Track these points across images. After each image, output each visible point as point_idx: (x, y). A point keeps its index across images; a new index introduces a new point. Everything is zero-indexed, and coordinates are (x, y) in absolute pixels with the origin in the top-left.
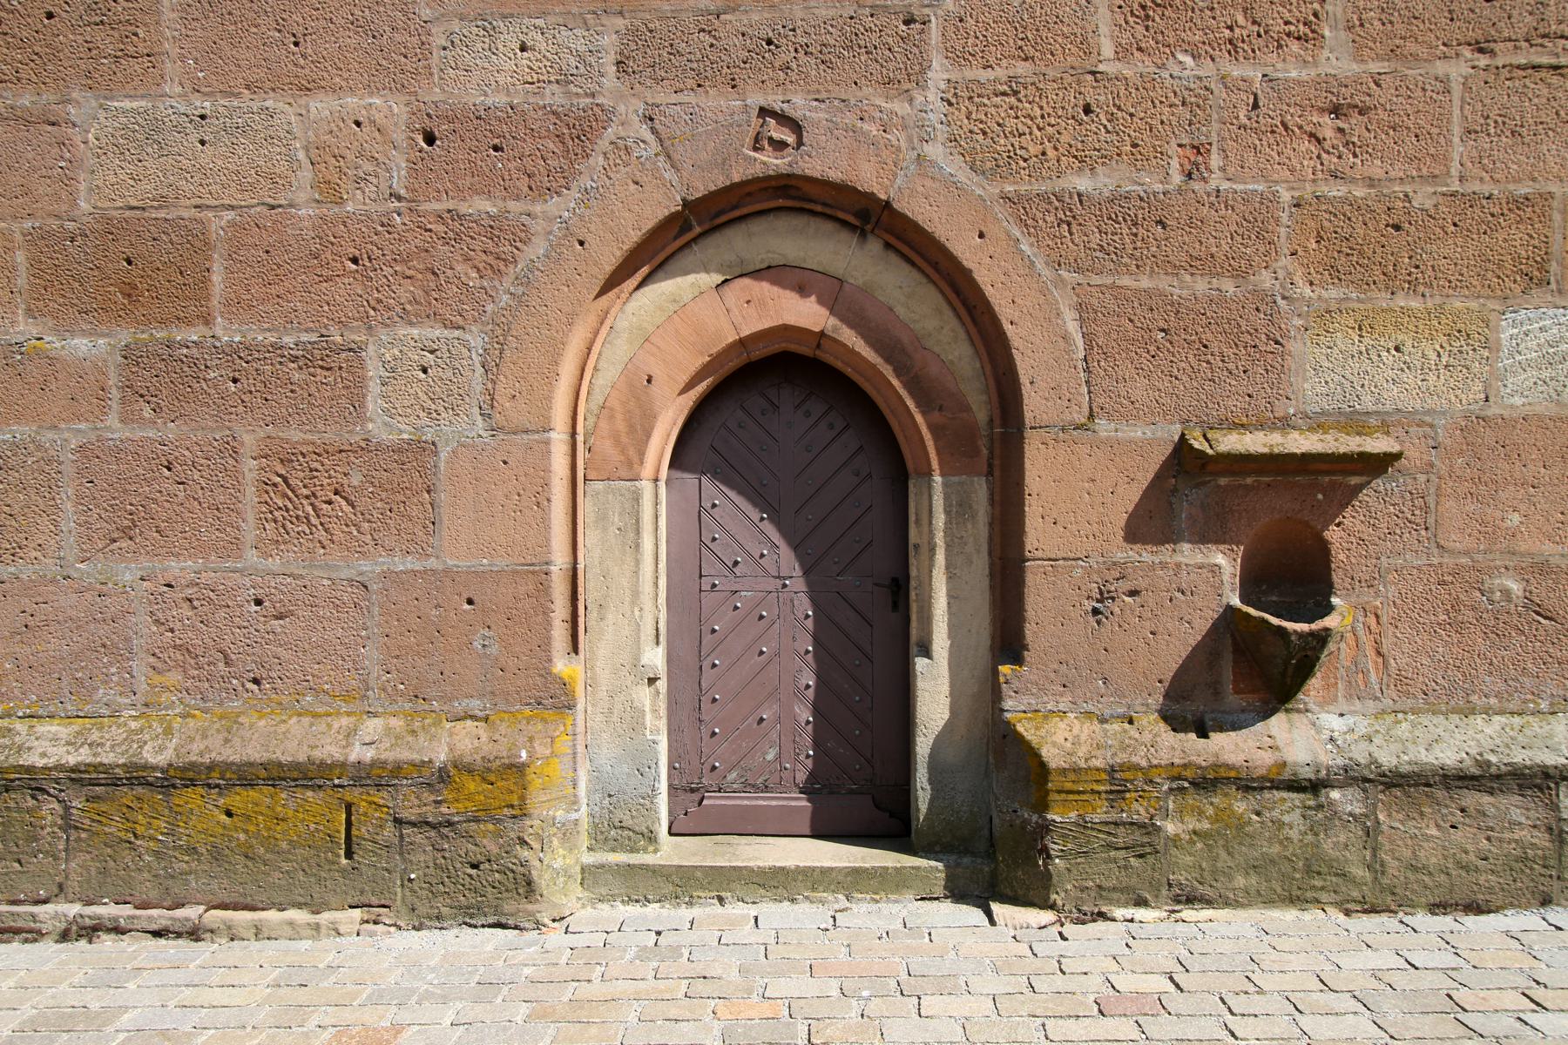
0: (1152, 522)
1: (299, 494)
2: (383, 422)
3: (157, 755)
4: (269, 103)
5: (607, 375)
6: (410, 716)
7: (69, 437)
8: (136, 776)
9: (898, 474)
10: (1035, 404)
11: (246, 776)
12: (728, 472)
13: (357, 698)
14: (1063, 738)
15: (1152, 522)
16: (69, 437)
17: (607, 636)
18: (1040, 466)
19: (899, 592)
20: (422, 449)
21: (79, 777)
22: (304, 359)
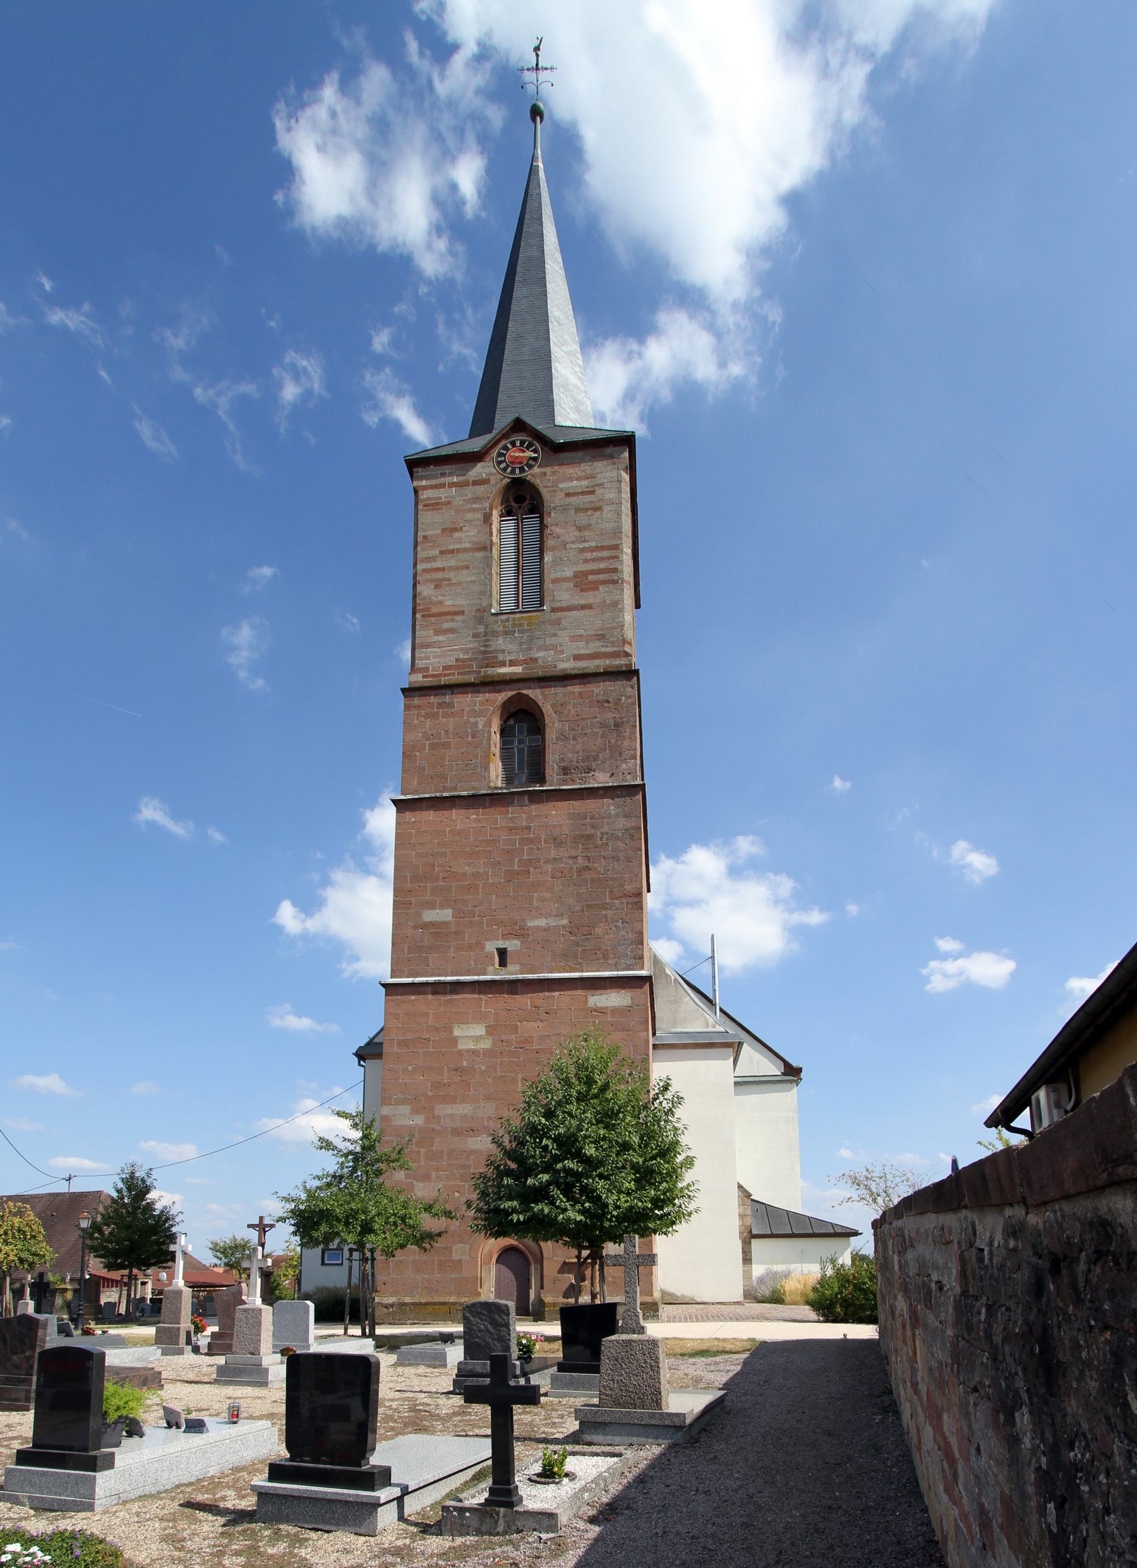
0: (561, 1271)
1: (442, 1266)
2: (455, 1257)
3: (423, 1301)
4: (640, 1204)
5: (486, 1250)
6: (1013, 1226)
7: (411, 1258)
8: (421, 1304)
9: (529, 1264)
10: (545, 1255)
11: (435, 1304)
12: (504, 1264)
13: (450, 1294)
14: (548, 1299)
15: (561, 1271)
16: (411, 1258)
17: (485, 1287)
18: (545, 1262)
19: (529, 1281)
20: (460, 1261)
21: (412, 1304)
22: (444, 1248)
